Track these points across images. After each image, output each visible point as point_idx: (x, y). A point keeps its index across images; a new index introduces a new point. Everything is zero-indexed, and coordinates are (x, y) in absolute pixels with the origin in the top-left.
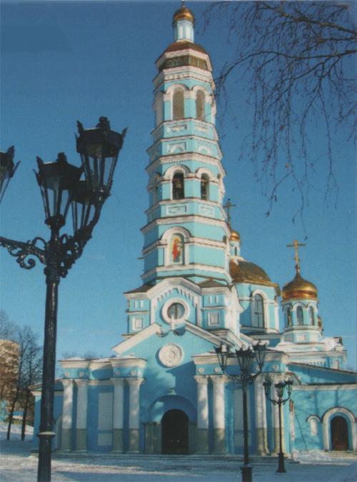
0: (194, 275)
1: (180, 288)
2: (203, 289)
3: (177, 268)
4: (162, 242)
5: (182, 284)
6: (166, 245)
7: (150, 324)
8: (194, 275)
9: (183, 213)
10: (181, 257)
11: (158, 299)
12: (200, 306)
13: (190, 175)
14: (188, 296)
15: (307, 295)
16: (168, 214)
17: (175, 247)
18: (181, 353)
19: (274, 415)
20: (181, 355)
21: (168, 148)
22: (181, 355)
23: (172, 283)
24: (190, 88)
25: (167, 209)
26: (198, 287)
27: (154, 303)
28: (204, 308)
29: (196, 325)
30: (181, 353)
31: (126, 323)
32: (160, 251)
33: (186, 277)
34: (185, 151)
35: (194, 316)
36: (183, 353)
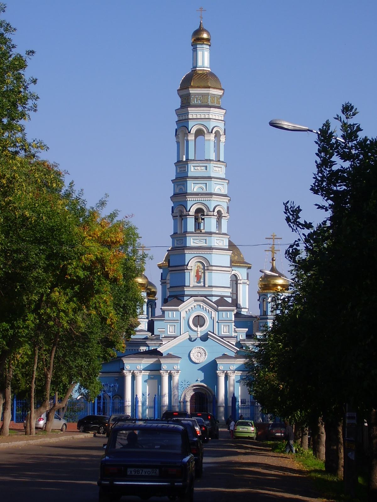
2: (219, 307)
4: (189, 268)
5: (203, 301)
6: (192, 270)
8: (212, 296)
10: (202, 280)
11: (186, 312)
12: (216, 320)
13: (210, 213)
17: (198, 272)
18: (205, 354)
19: (200, 490)
20: (205, 356)
21: (193, 187)
22: (205, 356)
27: (183, 314)
29: (213, 333)
30: (205, 354)
32: (187, 274)
33: (205, 296)
36: (207, 354)
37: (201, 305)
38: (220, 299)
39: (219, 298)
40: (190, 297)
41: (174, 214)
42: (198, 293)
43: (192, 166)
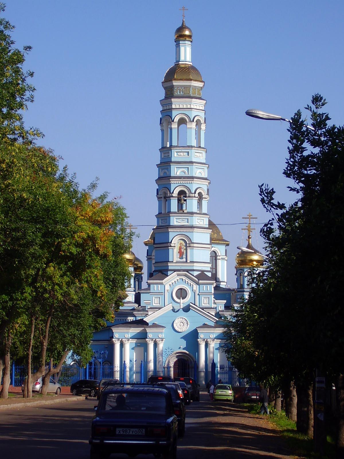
0: (194, 270)
1: (184, 278)
2: (200, 281)
4: (172, 245)
5: (186, 276)
6: (175, 247)
7: (165, 306)
8: (194, 270)
10: (184, 256)
11: (170, 285)
12: (197, 292)
13: (191, 195)
17: (180, 248)
18: (187, 323)
22: (187, 325)
25: (175, 219)
26: (196, 279)
27: (167, 287)
28: (199, 294)
29: (195, 305)
30: (187, 323)
32: (170, 251)
33: (187, 271)
35: (182, 61)
36: (189, 323)
37: (184, 278)
38: (200, 273)
39: (201, 272)
40: (173, 272)
41: (159, 196)
42: (181, 268)
43: (176, 152)
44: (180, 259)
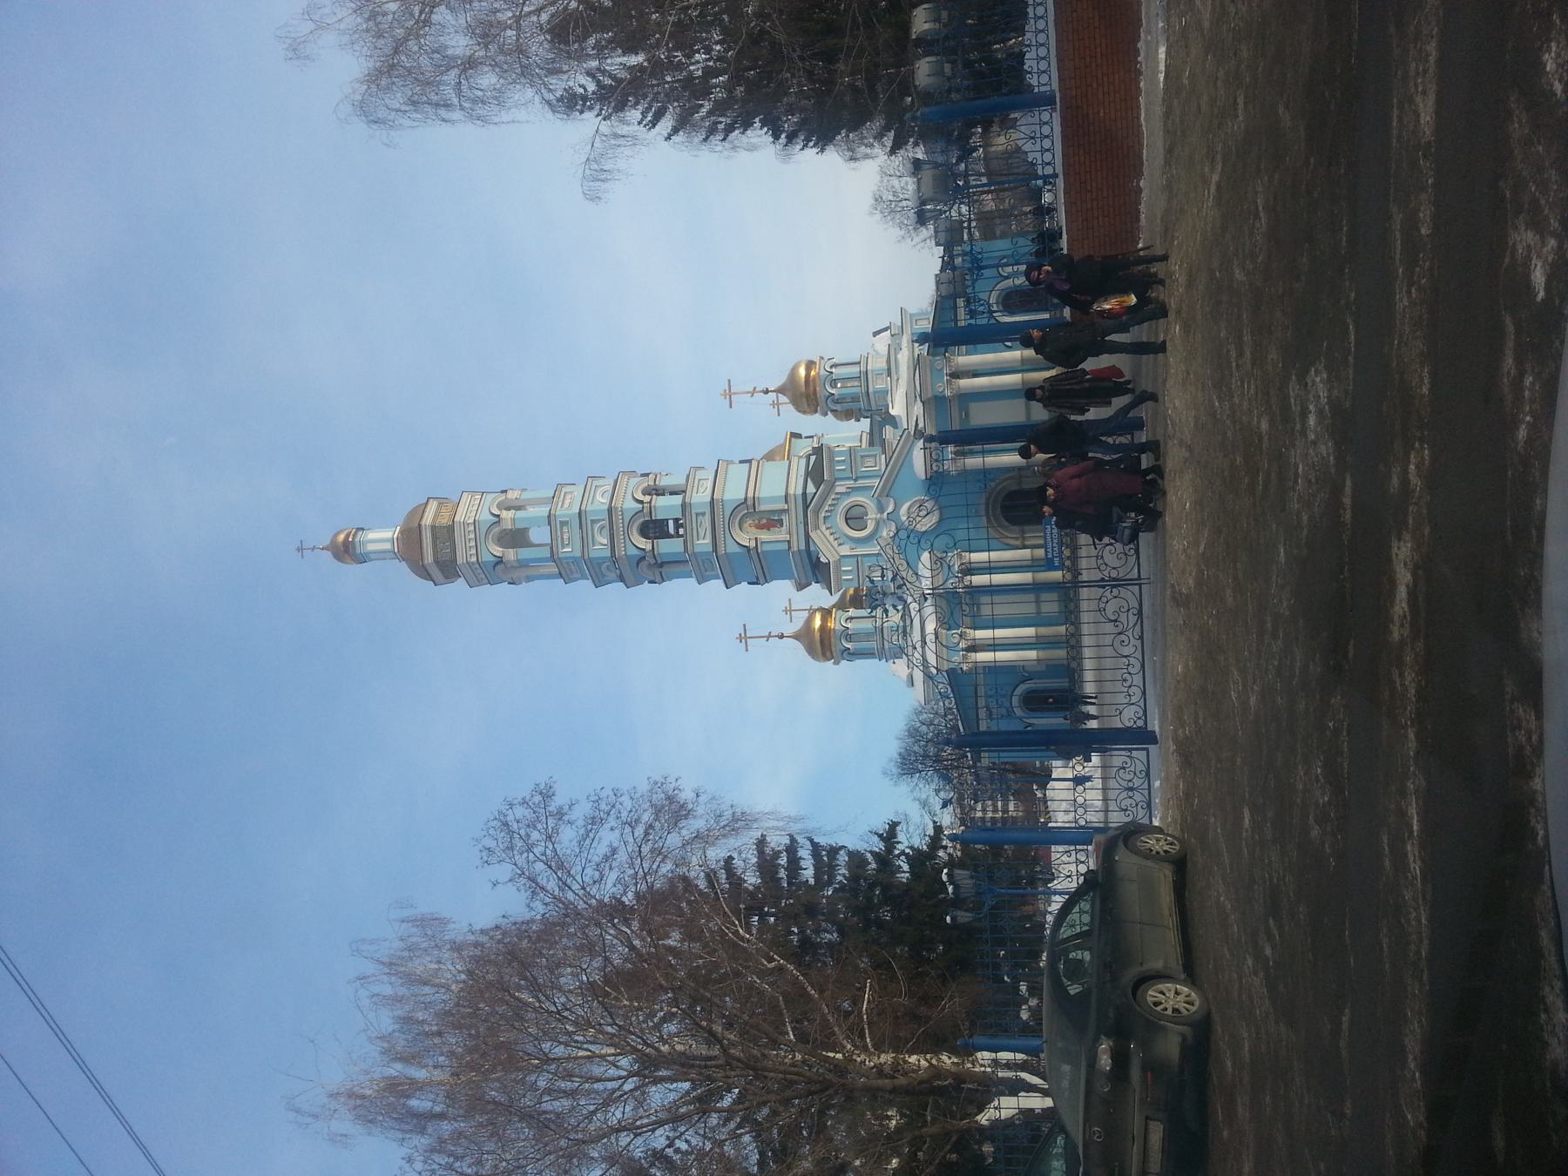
3: (792, 521)
5: (817, 513)
8: (804, 494)
9: (708, 518)
11: (840, 545)
14: (833, 502)
15: (813, 373)
16: (708, 540)
17: (760, 527)
23: (817, 527)
24: (496, 519)
31: (39, 1109)
32: (766, 548)
33: (806, 507)
34: (606, 523)
37: (823, 515)
38: (812, 480)
40: (811, 541)
44: (782, 525)
